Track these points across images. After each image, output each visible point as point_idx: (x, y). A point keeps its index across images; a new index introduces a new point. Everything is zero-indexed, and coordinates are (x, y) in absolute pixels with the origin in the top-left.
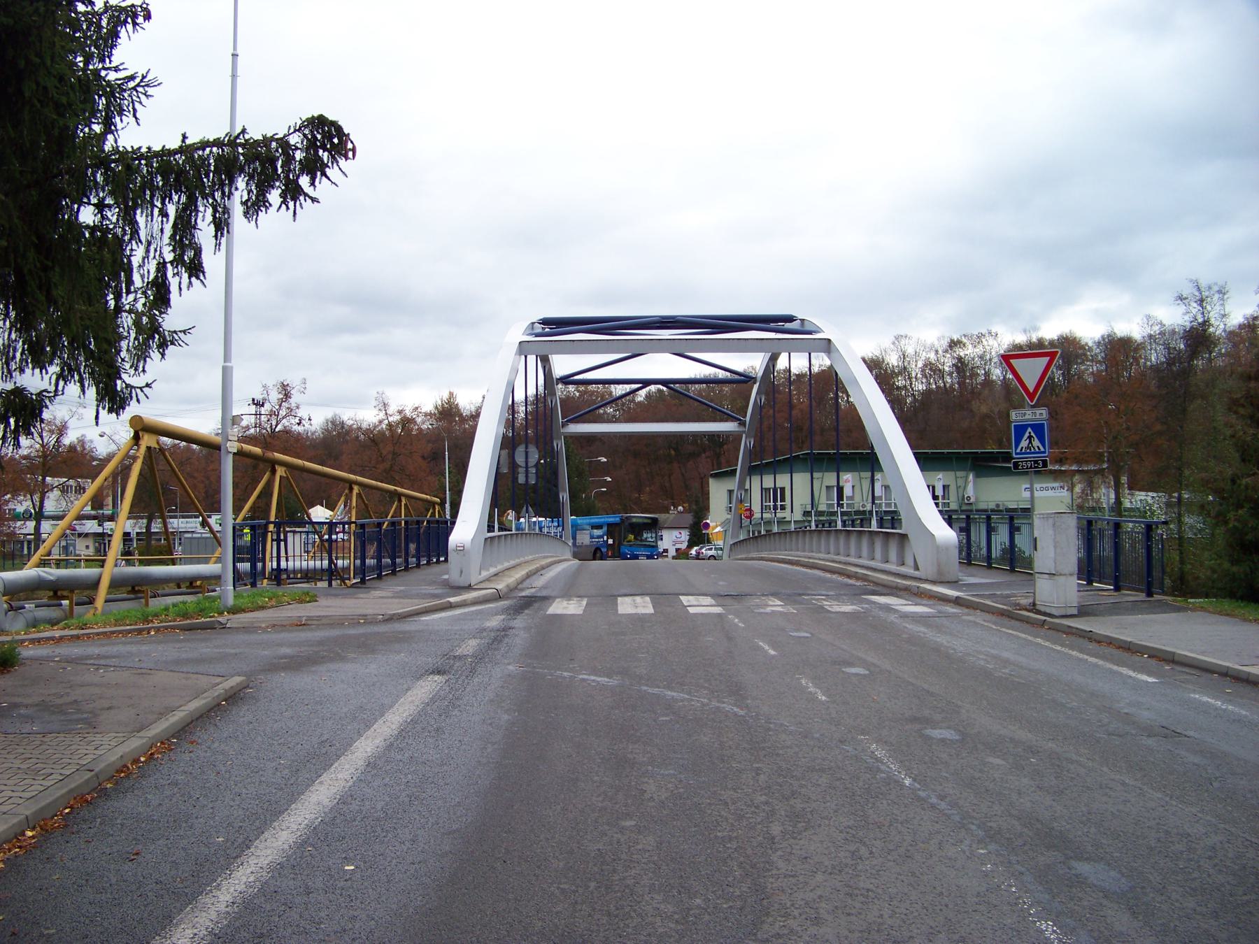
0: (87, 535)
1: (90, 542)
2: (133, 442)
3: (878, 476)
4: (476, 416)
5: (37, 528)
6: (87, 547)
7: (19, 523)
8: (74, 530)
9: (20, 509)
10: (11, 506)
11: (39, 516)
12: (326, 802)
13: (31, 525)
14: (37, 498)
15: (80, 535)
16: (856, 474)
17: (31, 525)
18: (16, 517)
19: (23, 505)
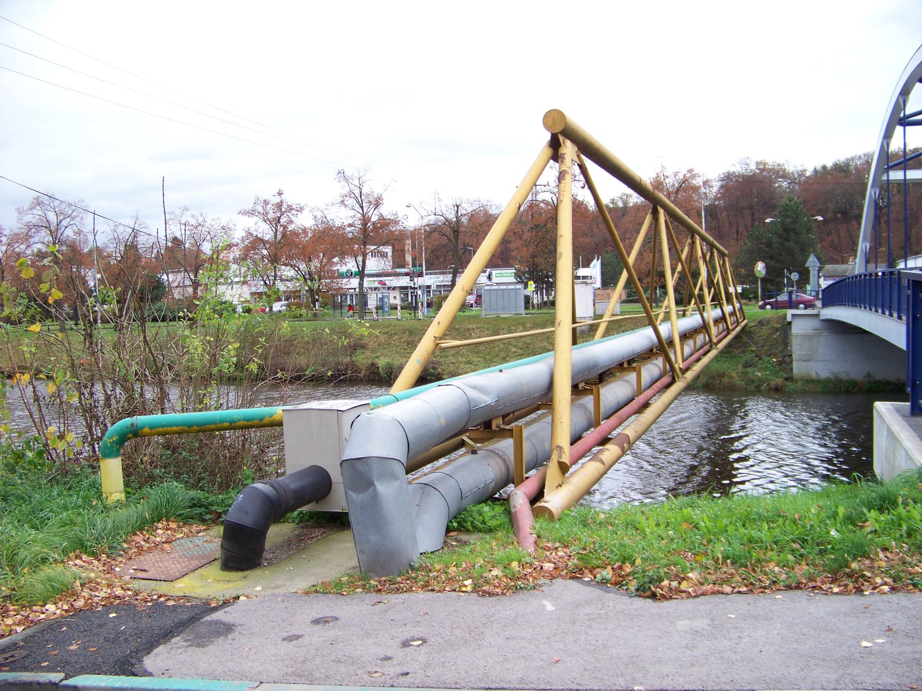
0: (394, 288)
1: (397, 293)
2: (549, 152)
3: (695, 497)
4: (556, 208)
5: (361, 285)
6: (395, 298)
7: (345, 280)
8: (385, 284)
9: (343, 269)
10: (338, 267)
11: (361, 274)
12: (383, 389)
13: (355, 282)
14: (360, 259)
15: (389, 288)
16: (218, 555)
17: (355, 282)
18: (341, 276)
19: (351, 265)
